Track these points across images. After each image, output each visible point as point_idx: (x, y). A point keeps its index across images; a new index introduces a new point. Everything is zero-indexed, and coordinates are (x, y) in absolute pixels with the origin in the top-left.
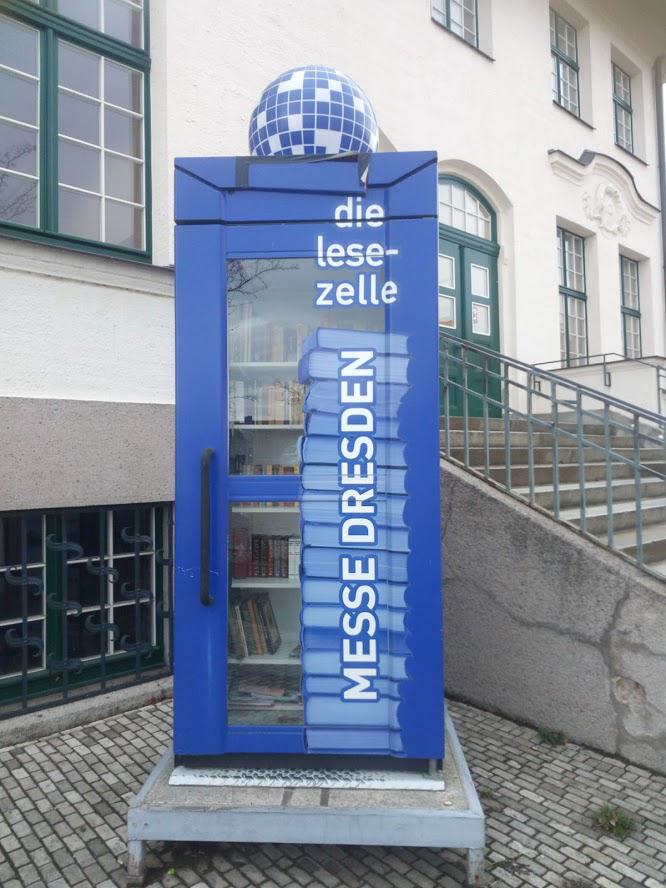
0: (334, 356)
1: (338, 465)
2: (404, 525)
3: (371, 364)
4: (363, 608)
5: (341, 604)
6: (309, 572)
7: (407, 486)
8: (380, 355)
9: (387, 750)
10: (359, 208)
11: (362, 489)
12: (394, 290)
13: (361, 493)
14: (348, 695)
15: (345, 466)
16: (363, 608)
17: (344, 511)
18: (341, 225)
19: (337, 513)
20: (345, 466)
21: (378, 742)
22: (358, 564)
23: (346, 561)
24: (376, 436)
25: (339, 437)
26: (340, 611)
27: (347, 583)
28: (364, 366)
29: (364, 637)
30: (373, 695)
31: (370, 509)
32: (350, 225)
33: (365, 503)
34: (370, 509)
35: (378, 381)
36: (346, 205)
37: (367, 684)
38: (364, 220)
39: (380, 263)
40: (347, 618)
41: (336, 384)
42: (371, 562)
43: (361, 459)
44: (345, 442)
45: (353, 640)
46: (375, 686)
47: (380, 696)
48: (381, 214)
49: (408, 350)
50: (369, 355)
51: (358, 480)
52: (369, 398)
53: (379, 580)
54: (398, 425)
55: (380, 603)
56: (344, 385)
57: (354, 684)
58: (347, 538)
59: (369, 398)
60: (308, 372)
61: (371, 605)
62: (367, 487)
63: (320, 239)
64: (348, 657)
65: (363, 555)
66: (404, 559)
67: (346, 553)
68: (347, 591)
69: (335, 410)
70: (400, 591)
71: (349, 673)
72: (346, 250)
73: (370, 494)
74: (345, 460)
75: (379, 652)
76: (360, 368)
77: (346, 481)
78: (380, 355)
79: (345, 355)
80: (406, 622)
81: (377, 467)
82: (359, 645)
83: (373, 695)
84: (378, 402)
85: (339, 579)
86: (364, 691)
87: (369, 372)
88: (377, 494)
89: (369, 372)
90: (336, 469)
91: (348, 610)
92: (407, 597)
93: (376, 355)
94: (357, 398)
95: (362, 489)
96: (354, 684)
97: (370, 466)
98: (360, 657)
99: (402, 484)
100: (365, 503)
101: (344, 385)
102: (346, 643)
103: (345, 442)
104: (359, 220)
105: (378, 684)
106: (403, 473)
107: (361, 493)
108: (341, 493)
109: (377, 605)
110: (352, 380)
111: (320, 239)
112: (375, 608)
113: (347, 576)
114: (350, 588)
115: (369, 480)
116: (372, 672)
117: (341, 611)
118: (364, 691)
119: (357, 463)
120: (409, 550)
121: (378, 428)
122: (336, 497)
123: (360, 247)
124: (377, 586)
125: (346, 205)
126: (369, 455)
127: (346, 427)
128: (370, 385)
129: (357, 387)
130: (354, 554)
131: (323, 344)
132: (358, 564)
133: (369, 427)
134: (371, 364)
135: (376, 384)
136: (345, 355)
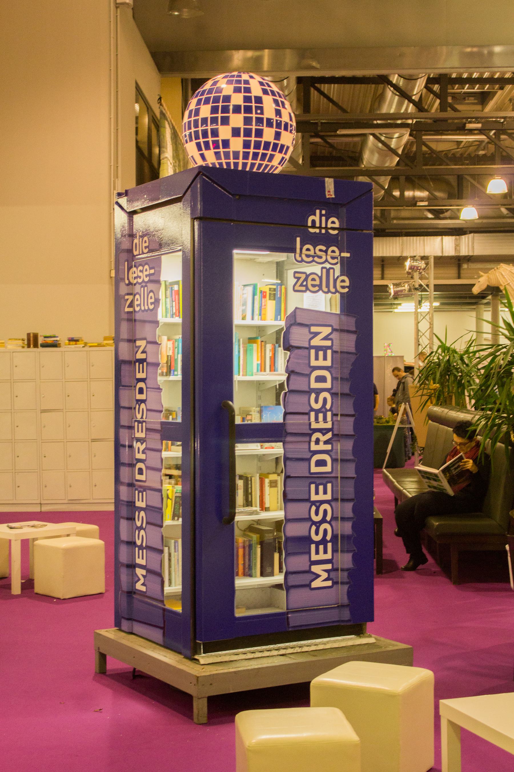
0: (305, 330)
1: (308, 414)
2: (352, 457)
3: (330, 337)
4: (324, 520)
5: (310, 519)
6: (290, 497)
7: (355, 429)
8: (336, 330)
9: (338, 621)
10: (324, 218)
11: (324, 432)
12: (347, 284)
13: (324, 434)
14: (314, 585)
15: (313, 414)
16: (324, 520)
17: (312, 365)
18: (312, 230)
19: (307, 450)
20: (313, 414)
21: (333, 616)
22: (321, 488)
23: (313, 486)
24: (332, 391)
25: (309, 392)
26: (310, 523)
27: (314, 503)
28: (326, 338)
29: (324, 542)
30: (329, 583)
31: (328, 447)
32: (317, 231)
33: (326, 442)
34: (328, 447)
35: (334, 349)
36: (315, 215)
37: (325, 575)
38: (326, 228)
39: (346, 290)
40: (314, 528)
41: (307, 351)
42: (329, 486)
43: (323, 410)
44: (313, 396)
45: (318, 544)
46: (331, 577)
47: (335, 583)
48: (337, 225)
49: (357, 327)
50: (328, 330)
51: (322, 425)
52: (328, 363)
53: (334, 499)
54: (350, 383)
55: (334, 516)
56: (313, 352)
57: (318, 576)
58: (314, 469)
59: (328, 363)
60: (289, 343)
61: (328, 518)
62: (327, 430)
63: (298, 239)
64: (314, 557)
65: (324, 481)
66: (352, 482)
67: (313, 480)
68: (314, 508)
69: (307, 372)
70: (349, 506)
71: (315, 569)
72: (315, 249)
73: (329, 435)
74: (312, 410)
75: (334, 551)
76: (323, 339)
77: (314, 426)
78: (336, 330)
79: (314, 329)
80: (353, 527)
81: (334, 415)
82: (321, 547)
83: (329, 583)
84: (334, 366)
85: (308, 500)
86: (323, 581)
87: (328, 343)
88: (333, 435)
89: (328, 343)
90: (306, 417)
91: (314, 523)
92: (354, 510)
93: (334, 330)
94: (321, 363)
95: (324, 432)
96: (318, 576)
97: (329, 414)
98: (321, 556)
99: (352, 428)
100: (326, 442)
101: (313, 352)
102: (313, 546)
103: (313, 396)
104: (323, 228)
105: (333, 575)
106: (352, 419)
107: (324, 434)
108: (310, 435)
109: (333, 518)
110: (318, 349)
111: (298, 239)
112: (331, 520)
113: (314, 498)
114: (316, 506)
115: (329, 425)
116: (329, 566)
117: (310, 523)
118: (323, 581)
119: (321, 412)
120: (356, 476)
121: (334, 385)
122: (307, 439)
123: (324, 248)
124: (333, 504)
125: (315, 215)
126: (328, 406)
127: (314, 385)
128: (329, 352)
129: (321, 353)
130: (318, 481)
131: (299, 320)
132: (321, 488)
133: (328, 385)
134: (330, 337)
135: (334, 352)
136: (314, 329)
